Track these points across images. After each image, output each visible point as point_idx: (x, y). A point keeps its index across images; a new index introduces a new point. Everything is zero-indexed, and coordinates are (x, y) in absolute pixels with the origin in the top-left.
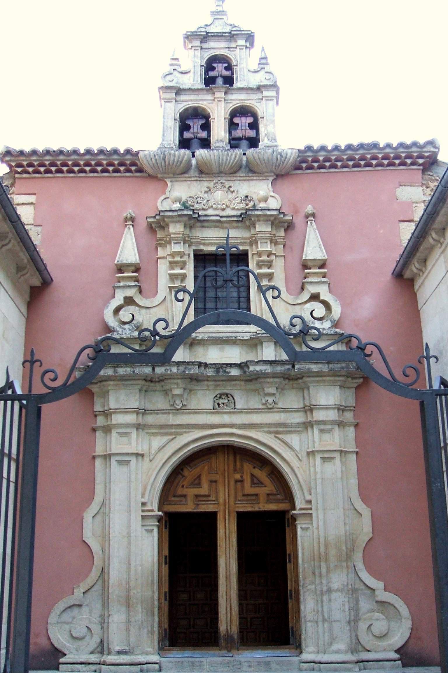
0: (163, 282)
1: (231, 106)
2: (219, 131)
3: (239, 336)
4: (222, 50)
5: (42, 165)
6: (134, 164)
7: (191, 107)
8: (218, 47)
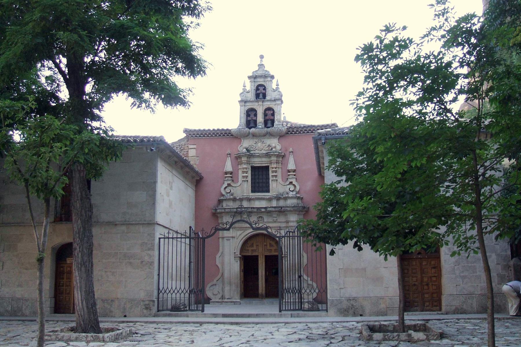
0: (240, 179)
1: (265, 108)
2: (260, 119)
3: (265, 197)
5: (198, 134)
6: (230, 133)
8: (260, 81)
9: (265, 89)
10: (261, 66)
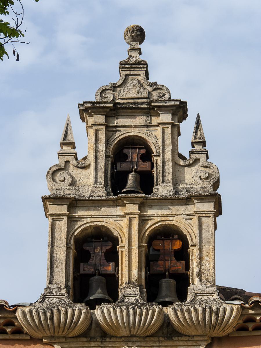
2: (129, 269)
4: (137, 130)
7: (90, 226)
8: (131, 126)
10: (134, 67)
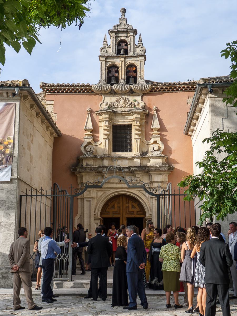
2: (122, 75)
8: (122, 36)
9: (126, 45)
10: (123, 20)
